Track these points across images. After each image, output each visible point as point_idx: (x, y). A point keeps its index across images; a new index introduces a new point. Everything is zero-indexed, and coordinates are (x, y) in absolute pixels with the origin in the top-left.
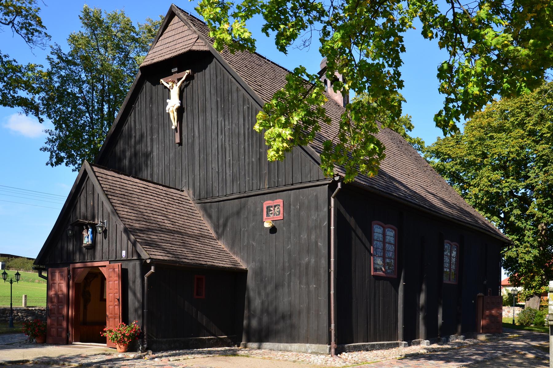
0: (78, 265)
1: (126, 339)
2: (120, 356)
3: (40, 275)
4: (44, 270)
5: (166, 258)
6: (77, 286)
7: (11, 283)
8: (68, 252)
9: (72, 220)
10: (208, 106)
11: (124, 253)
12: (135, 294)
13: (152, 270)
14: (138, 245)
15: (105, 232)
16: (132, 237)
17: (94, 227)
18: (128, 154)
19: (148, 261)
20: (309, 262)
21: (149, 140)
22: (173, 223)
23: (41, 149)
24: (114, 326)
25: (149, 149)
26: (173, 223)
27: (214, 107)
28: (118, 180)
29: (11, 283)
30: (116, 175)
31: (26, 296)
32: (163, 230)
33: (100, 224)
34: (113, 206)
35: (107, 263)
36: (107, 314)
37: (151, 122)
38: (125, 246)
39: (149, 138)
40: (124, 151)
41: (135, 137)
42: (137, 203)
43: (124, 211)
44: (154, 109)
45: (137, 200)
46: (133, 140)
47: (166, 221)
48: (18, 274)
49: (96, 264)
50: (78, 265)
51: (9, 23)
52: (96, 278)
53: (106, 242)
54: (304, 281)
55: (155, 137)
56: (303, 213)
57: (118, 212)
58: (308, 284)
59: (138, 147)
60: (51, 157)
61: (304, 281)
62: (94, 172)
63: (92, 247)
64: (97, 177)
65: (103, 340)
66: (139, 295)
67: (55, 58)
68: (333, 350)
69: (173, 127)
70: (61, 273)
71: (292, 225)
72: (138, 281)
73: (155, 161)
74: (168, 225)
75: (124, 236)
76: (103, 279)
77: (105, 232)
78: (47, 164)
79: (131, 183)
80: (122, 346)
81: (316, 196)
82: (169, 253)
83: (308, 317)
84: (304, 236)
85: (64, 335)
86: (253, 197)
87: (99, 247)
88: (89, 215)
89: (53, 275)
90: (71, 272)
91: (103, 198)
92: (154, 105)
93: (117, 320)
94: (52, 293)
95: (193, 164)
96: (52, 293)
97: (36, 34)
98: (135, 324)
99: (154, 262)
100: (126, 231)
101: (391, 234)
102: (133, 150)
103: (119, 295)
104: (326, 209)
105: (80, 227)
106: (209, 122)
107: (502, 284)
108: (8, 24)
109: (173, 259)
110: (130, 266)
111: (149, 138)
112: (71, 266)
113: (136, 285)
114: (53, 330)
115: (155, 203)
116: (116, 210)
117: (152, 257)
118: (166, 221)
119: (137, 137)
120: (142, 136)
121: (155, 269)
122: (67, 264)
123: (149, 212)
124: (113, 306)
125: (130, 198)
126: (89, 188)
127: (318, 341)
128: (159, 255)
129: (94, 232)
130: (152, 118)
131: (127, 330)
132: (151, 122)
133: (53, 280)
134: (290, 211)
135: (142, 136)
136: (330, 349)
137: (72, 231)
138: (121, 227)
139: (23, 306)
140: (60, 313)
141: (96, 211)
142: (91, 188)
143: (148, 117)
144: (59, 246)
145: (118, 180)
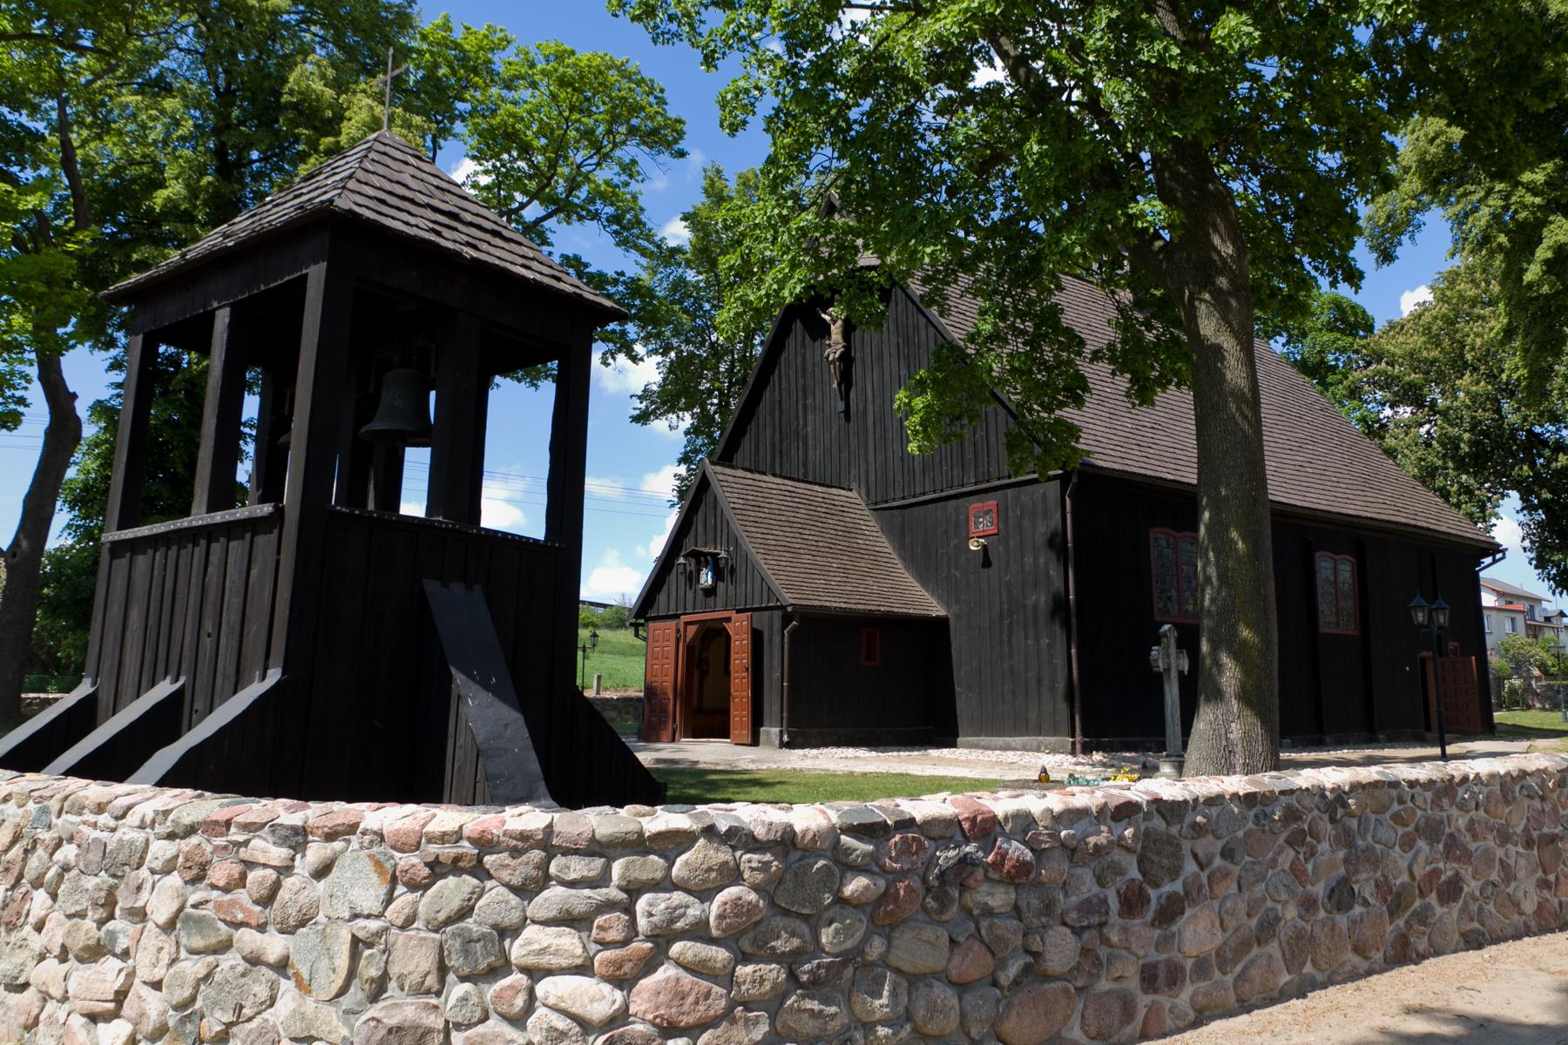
3: (637, 635)
10: (886, 351)
20: (1038, 601)
27: (894, 351)
35: (733, 614)
37: (804, 377)
44: (808, 356)
54: (1031, 633)
55: (809, 401)
56: (1026, 523)
58: (1037, 639)
61: (1031, 633)
68: (1078, 747)
71: (1011, 542)
76: (729, 637)
81: (1044, 494)
83: (1039, 693)
84: (1029, 560)
86: (930, 506)
95: (866, 445)
101: (1346, 571)
104: (1058, 516)
106: (887, 378)
107: (244, 419)
127: (1055, 732)
132: (804, 377)
134: (1007, 519)
136: (1073, 744)
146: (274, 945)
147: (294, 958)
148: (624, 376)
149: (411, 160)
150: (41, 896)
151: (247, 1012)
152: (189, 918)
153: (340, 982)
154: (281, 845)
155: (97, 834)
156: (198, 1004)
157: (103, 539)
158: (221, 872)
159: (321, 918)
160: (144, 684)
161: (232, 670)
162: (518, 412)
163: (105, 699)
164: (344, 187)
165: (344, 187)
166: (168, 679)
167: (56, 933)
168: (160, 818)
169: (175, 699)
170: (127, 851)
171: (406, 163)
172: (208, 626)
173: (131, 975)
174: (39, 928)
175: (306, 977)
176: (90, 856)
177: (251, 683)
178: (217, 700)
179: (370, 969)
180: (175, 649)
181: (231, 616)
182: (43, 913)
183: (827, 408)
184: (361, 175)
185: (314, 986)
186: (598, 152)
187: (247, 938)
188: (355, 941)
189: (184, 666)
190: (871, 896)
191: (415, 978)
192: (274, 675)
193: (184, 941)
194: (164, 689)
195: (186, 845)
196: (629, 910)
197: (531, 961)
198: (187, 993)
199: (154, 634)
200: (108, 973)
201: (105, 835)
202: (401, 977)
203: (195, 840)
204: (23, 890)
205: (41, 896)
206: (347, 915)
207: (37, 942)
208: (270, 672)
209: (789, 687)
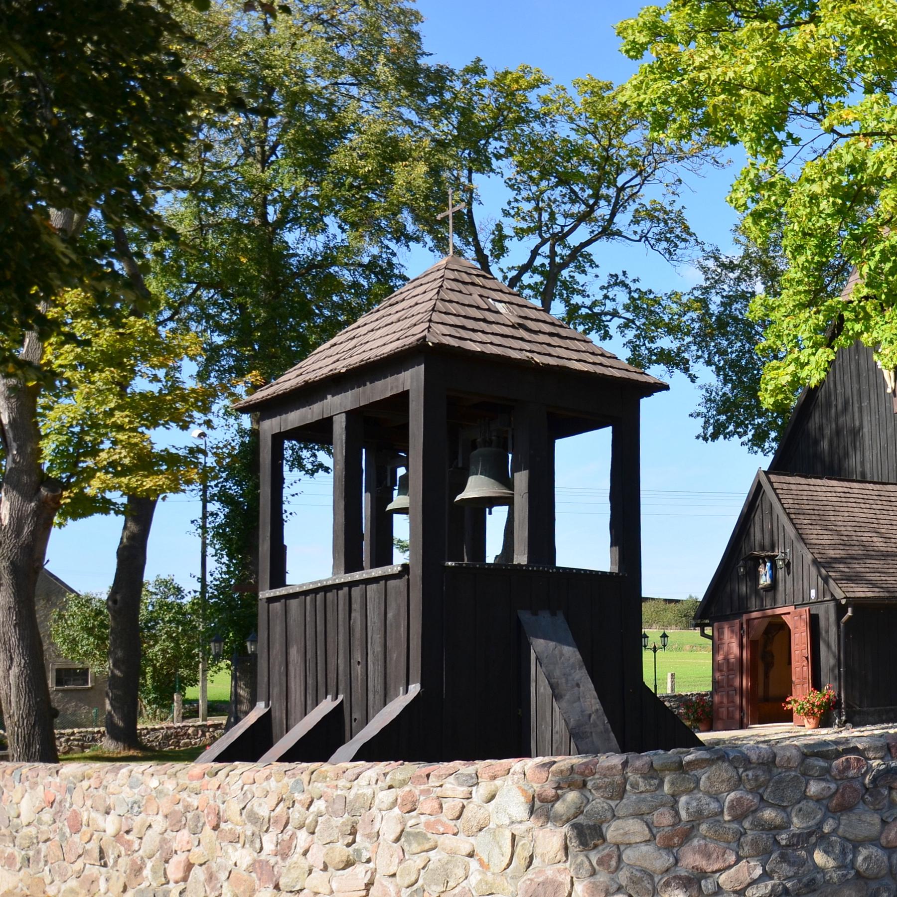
0: (754, 615)
1: (816, 710)
2: (809, 732)
3: (703, 634)
4: (708, 625)
5: (870, 595)
6: (753, 645)
7: (655, 651)
8: (740, 597)
9: (745, 550)
11: (813, 593)
12: (828, 646)
13: (849, 614)
14: (831, 582)
15: (788, 565)
16: (823, 571)
17: (773, 559)
18: (827, 432)
19: (843, 602)
21: (856, 409)
22: (886, 539)
23: (691, 415)
24: (802, 695)
25: (857, 424)
26: (886, 539)
28: (806, 487)
29: (655, 651)
30: (802, 480)
31: (672, 675)
32: (869, 554)
33: (780, 556)
34: (797, 529)
35: (791, 609)
36: (794, 679)
37: (859, 382)
38: (814, 583)
39: (856, 406)
40: (821, 428)
41: (836, 406)
42: (833, 518)
43: (815, 534)
44: (862, 362)
45: (832, 513)
46: (833, 411)
47: (875, 539)
48: (664, 636)
49: (779, 611)
50: (754, 615)
51: (641, 238)
52: (778, 629)
53: (789, 579)
55: (865, 404)
57: (804, 536)
59: (841, 420)
60: (705, 428)
62: (771, 483)
63: (773, 586)
64: (775, 490)
65: (787, 717)
66: (834, 648)
67: (711, 264)
69: (889, 391)
70: (731, 627)
72: (833, 630)
73: (867, 442)
74: (879, 543)
75: (813, 570)
77: (788, 565)
78: (698, 437)
79: (824, 489)
80: (811, 720)
82: (875, 585)
85: (737, 716)
87: (781, 587)
88: (767, 542)
89: (721, 633)
90: (745, 626)
91: (784, 519)
92: (862, 357)
93: (806, 686)
94: (720, 658)
96: (720, 658)
97: (682, 245)
98: (830, 690)
99: (851, 601)
100: (815, 562)
102: (834, 426)
103: (807, 652)
105: (757, 561)
108: (640, 240)
109: (882, 594)
110: (820, 610)
111: (856, 406)
112: (745, 617)
113: (831, 633)
114: (723, 711)
115: (861, 514)
116: (800, 535)
117: (848, 595)
118: (875, 539)
119: (840, 407)
120: (846, 403)
121: (853, 612)
122: (739, 615)
123: (849, 529)
124: (800, 668)
125: (821, 513)
126: (766, 507)
128: (861, 592)
129: (774, 568)
130: (859, 375)
131: (817, 698)
132: (859, 382)
133: (720, 639)
135: (846, 403)
137: (745, 567)
138: (809, 557)
139: (669, 691)
140: (730, 684)
141: (776, 538)
142: (768, 506)
143: (854, 373)
144: (728, 589)
145: (806, 487)
146: (464, 844)
147: (477, 851)
148: (671, 418)
149: (477, 280)
150: (303, 835)
151: (452, 884)
152: (409, 834)
153: (507, 861)
154: (462, 785)
155: (339, 792)
156: (420, 882)
157: (261, 596)
158: (427, 805)
159: (492, 826)
160: (309, 702)
161: (380, 687)
162: (582, 462)
163: (278, 715)
164: (430, 321)
165: (430, 321)
166: (329, 697)
167: (317, 856)
168: (382, 777)
169: (337, 712)
170: (361, 800)
171: (473, 284)
172: (357, 656)
173: (374, 872)
174: (305, 853)
175: (486, 860)
176: (336, 806)
177: (397, 695)
178: (371, 711)
179: (522, 854)
180: (332, 675)
181: (375, 648)
182: (307, 846)
183: (882, 410)
184: (440, 305)
185: (491, 865)
186: (640, 173)
187: (447, 841)
188: (514, 837)
189: (341, 687)
190: (826, 793)
191: (551, 854)
192: (415, 689)
193: (406, 848)
194: (327, 706)
195: (400, 792)
196: (674, 807)
197: (619, 839)
198: (413, 879)
199: (313, 665)
200: (359, 873)
201: (344, 793)
202: (542, 855)
203: (407, 789)
204: (290, 833)
205: (303, 835)
206: (507, 822)
207: (305, 864)
208: (411, 687)
209: (846, 672)
